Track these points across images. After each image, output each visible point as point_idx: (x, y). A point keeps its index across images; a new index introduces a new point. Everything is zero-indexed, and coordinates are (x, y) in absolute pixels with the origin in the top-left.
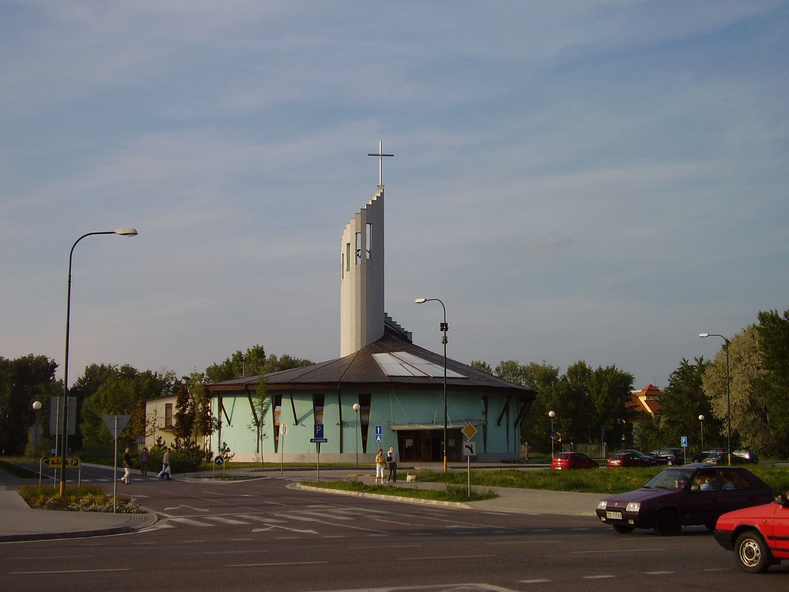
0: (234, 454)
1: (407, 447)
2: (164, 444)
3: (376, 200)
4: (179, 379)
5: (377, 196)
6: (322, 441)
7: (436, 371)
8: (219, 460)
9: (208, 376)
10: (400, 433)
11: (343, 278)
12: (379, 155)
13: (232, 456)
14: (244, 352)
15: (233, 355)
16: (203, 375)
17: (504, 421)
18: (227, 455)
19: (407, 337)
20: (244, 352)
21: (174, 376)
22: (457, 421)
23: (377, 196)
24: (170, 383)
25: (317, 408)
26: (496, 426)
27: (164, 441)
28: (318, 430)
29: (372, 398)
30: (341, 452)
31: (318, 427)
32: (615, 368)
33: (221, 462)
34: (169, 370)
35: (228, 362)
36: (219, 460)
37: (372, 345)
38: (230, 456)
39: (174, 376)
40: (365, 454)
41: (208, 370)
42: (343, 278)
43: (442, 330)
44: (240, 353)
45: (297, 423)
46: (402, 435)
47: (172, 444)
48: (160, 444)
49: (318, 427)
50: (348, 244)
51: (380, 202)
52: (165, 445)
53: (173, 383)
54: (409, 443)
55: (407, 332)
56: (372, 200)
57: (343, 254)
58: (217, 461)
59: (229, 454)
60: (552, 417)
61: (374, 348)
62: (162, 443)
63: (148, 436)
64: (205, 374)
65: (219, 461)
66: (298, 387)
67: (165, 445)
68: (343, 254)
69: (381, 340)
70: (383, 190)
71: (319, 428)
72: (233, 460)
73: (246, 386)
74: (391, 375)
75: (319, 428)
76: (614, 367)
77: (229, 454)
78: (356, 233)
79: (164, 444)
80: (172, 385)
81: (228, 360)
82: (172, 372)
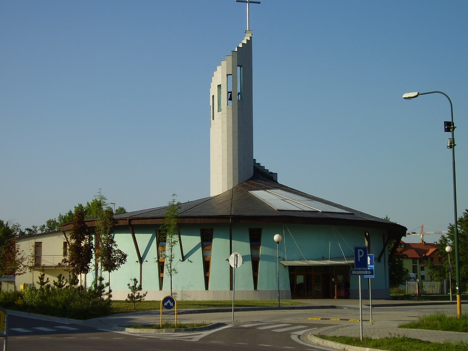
0: (147, 293)
1: (297, 283)
2: (47, 282)
3: (246, 43)
4: (23, 231)
5: (247, 40)
6: (366, 272)
7: (302, 210)
8: (169, 301)
9: (48, 227)
10: (292, 269)
11: (213, 119)
12: (247, 2)
13: (145, 295)
14: (85, 205)
15: (75, 207)
16: (44, 226)
17: (382, 259)
18: (139, 293)
19: (273, 178)
20: (85, 205)
21: (19, 228)
22: (319, 259)
23: (247, 40)
24: (16, 233)
25: (205, 243)
26: (377, 263)
27: (48, 279)
28: (359, 256)
29: (262, 231)
30: (231, 288)
31: (359, 250)
32: (388, 219)
33: (172, 304)
34: (15, 223)
35: (70, 213)
36: (169, 301)
37: (244, 183)
38: (142, 295)
39: (19, 228)
40: (207, 291)
41: (49, 222)
42: (213, 119)
43: (447, 130)
44: (81, 205)
45: (184, 258)
46: (293, 270)
47: (54, 281)
48: (42, 282)
49: (359, 250)
50: (219, 86)
51: (248, 45)
52: (49, 283)
53: (18, 233)
54: (300, 279)
55: (272, 173)
56: (242, 43)
57: (213, 96)
58: (166, 304)
59: (141, 293)
60: (449, 253)
61: (247, 186)
62: (45, 280)
63: (20, 274)
64: (46, 225)
65: (169, 304)
66: (187, 221)
67: (49, 283)
68: (213, 96)
69: (251, 179)
70: (252, 34)
71: (361, 253)
72: (146, 298)
73: (130, 220)
74: (280, 209)
75: (361, 253)
76: (387, 218)
77: (141, 293)
78: (227, 75)
79: (47, 282)
80: (18, 235)
81: (71, 212)
82: (17, 225)
